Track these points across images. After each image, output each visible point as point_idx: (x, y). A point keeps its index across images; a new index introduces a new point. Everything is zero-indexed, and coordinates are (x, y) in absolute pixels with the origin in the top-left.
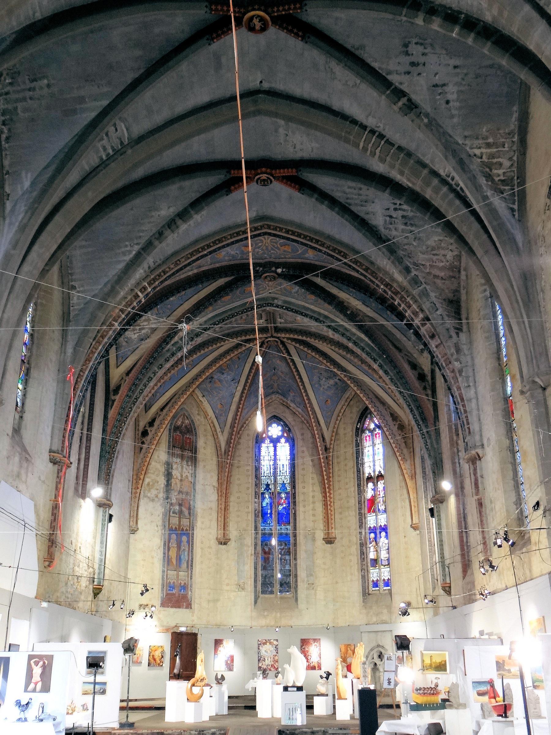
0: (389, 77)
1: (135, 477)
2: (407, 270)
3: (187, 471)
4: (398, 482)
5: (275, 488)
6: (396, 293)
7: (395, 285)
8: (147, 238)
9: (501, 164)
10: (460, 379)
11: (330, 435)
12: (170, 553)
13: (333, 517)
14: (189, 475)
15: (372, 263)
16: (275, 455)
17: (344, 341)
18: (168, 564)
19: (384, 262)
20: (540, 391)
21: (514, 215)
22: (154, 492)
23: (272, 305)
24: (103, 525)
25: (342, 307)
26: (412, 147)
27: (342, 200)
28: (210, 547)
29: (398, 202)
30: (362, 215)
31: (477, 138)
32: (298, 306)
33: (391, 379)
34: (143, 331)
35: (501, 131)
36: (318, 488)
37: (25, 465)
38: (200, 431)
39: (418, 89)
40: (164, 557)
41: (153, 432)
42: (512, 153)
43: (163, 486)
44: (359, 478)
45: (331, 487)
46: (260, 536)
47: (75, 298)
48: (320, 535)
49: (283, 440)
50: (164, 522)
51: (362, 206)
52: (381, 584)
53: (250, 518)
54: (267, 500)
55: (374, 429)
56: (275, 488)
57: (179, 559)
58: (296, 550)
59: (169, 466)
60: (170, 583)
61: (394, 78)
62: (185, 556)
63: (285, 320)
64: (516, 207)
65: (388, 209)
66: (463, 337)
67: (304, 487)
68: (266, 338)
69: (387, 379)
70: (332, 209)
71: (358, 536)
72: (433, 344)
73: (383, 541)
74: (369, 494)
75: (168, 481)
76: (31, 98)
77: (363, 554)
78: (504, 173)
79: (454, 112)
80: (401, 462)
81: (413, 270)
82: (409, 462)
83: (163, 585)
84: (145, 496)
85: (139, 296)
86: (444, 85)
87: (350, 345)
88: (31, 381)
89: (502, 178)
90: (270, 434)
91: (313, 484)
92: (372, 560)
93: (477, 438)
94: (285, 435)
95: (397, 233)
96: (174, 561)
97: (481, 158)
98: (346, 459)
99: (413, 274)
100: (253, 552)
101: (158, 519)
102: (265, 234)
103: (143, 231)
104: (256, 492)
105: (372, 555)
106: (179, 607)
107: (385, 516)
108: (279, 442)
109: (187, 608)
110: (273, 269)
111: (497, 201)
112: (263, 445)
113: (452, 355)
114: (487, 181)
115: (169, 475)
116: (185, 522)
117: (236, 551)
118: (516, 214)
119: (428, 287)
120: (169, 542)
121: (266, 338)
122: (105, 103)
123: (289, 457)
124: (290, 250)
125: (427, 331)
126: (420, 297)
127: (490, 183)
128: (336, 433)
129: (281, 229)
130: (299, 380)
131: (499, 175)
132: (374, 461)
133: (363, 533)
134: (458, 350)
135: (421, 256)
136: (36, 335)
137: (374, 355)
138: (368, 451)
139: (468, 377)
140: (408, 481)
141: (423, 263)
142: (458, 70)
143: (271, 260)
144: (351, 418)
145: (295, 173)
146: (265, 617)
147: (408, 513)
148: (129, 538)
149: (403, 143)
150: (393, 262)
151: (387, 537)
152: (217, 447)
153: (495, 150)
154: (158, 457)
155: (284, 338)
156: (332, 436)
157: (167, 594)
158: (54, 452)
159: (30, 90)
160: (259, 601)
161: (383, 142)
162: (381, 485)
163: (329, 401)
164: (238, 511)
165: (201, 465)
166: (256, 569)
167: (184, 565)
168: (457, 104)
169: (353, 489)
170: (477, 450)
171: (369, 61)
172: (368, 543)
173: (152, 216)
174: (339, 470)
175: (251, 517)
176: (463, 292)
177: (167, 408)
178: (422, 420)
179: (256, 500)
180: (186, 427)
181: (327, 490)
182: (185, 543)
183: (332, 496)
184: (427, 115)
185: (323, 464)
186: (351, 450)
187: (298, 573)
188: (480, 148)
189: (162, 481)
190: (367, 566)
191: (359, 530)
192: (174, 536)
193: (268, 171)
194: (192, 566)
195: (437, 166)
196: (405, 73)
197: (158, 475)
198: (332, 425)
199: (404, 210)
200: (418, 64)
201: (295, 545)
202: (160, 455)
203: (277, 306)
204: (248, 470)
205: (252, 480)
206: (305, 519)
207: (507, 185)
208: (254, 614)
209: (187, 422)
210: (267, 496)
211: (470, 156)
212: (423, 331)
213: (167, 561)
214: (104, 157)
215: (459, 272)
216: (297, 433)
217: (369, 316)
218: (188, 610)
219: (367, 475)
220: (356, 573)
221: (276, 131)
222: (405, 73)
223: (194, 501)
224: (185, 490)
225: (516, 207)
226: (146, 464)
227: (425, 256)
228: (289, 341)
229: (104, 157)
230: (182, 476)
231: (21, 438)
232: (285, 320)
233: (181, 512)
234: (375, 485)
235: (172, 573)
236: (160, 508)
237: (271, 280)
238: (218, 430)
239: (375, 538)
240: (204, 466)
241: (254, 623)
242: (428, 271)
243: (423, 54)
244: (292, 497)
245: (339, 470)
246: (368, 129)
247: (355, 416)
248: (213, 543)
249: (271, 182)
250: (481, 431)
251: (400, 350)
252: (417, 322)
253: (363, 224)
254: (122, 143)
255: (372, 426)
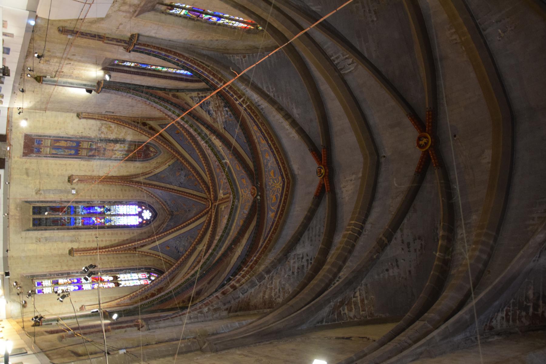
0: (399, 231)
1: (115, 117)
2: (268, 272)
3: (119, 155)
4: (114, 295)
5: (108, 215)
6: (251, 268)
7: (257, 266)
8: (278, 101)
9: (351, 310)
10: (196, 312)
11: (145, 251)
12: (63, 142)
13: (88, 254)
14: (116, 156)
15: (270, 251)
16: (130, 215)
17: (213, 247)
18: (55, 140)
19: (271, 257)
20: (198, 347)
21: (318, 323)
22: (104, 129)
23: (234, 198)
24: (85, 85)
25: (236, 241)
26: (355, 253)
27: (311, 225)
28: (66, 170)
29: (312, 262)
30: (302, 239)
31: (366, 293)
32: (235, 215)
33: (188, 279)
34: (214, 113)
35: (372, 308)
36: (108, 243)
37: (132, 10)
38: (146, 164)
39: (394, 250)
40: (60, 137)
41: (146, 129)
42: (358, 317)
43: (109, 137)
44: (116, 271)
45: (109, 253)
46: (74, 205)
47: (238, 58)
48: (75, 246)
49: (140, 220)
50: (85, 137)
51: (308, 238)
52: (40, 288)
53: (87, 198)
54: (99, 210)
55: (150, 279)
56: (108, 215)
57: (59, 148)
58: (64, 229)
59: (123, 141)
60: (42, 141)
61: (398, 234)
62: (60, 152)
63: (223, 211)
64: (324, 324)
65: (307, 256)
66: (225, 313)
67: (108, 234)
68: (211, 200)
69: (188, 276)
70: (305, 218)
71: (75, 271)
72: (218, 294)
73: (72, 288)
74: (105, 278)
75: (112, 141)
76: (364, 11)
77: (62, 275)
78: (345, 314)
79: (381, 275)
80: (129, 296)
81: (268, 276)
82: (129, 301)
83: (40, 136)
84: (102, 124)
85: (240, 99)
86: (398, 266)
87: (210, 251)
88: (185, 21)
89: (342, 312)
90: (145, 211)
91: (111, 241)
92: (58, 281)
93: (154, 326)
94: (144, 222)
95: (293, 263)
96: (57, 144)
97: (354, 297)
98: (129, 262)
99: (266, 276)
100: (63, 200)
101: (87, 133)
102: (284, 182)
103: (282, 99)
104: (105, 202)
105: (61, 281)
106: (24, 148)
107: (90, 288)
108: (139, 217)
109: (24, 153)
110: (259, 194)
111: (327, 310)
112: (137, 207)
113: (212, 306)
114: (340, 302)
115: (116, 141)
116: (84, 153)
117: (63, 189)
118: (320, 324)
119: (257, 287)
120: (71, 141)
121: (211, 200)
122: (366, 55)
123: (129, 224)
124: (273, 202)
125: (227, 289)
126: (250, 282)
127: (338, 304)
128: (146, 255)
129: (287, 191)
130: (182, 225)
131: (344, 310)
132: (128, 280)
133: (77, 275)
134: (216, 310)
135: (278, 281)
136: (215, 26)
137: (205, 267)
138: (135, 276)
139: (197, 318)
140: (116, 301)
141: (273, 283)
142: (408, 273)
143: (265, 192)
144: (157, 265)
145: (327, 189)
146: (16, 208)
147: (92, 303)
148: (74, 112)
149: (358, 248)
150: (273, 261)
151: (75, 290)
152: (137, 176)
153: (360, 305)
154: (129, 134)
155: (211, 212)
156: (144, 252)
157: (34, 139)
158: (138, 37)
159: (369, 10)
160: (28, 204)
161: (356, 234)
162: (112, 285)
163: (168, 249)
164: (92, 190)
165: (122, 164)
166: (51, 202)
167: (54, 152)
168: (386, 276)
169: (108, 267)
170: (145, 326)
171: (408, 217)
172: (70, 278)
173: (292, 104)
174: (121, 258)
175: (87, 198)
176: (256, 312)
177: (161, 138)
178: (161, 301)
179: (99, 202)
180: (149, 154)
181: (107, 250)
182: (70, 152)
183: (103, 253)
184: (378, 258)
185: (125, 246)
186: (136, 264)
187: (48, 231)
188: (360, 295)
189: (112, 136)
190: (53, 278)
191: (79, 271)
192: (75, 144)
193: (327, 174)
194: (53, 157)
195: (345, 270)
196: (402, 240)
197: (116, 133)
198: (152, 252)
199: (307, 266)
200: (409, 248)
201: (68, 229)
202: (130, 135)
203: (233, 202)
204: (119, 196)
205: (113, 199)
206: (86, 235)
207: (337, 316)
208: (18, 201)
209: (152, 154)
210: (102, 210)
211: (355, 289)
212: (227, 287)
213: (57, 139)
214: (332, 58)
215: (269, 308)
216: (145, 229)
217: (231, 260)
218: (22, 154)
219: (118, 276)
220: (48, 271)
221: (353, 174)
222: (402, 240)
223: (99, 159)
224: (106, 153)
225: (324, 324)
226: (124, 124)
227: (278, 283)
228: (209, 216)
229: (332, 58)
230: (116, 150)
231: (149, 11)
232: (223, 211)
233: (91, 150)
234: (111, 281)
235: (49, 142)
236: (94, 135)
237: (251, 192)
238: (147, 176)
239: (74, 283)
240: (122, 167)
241: (11, 201)
242: (268, 286)
243: (415, 250)
244: (102, 227)
245: (121, 258)
246: (363, 225)
247: (158, 267)
248: (70, 173)
249: (320, 176)
250: (160, 328)
251: (209, 283)
252: (232, 283)
253: (296, 239)
254: (341, 69)
255: (153, 278)
